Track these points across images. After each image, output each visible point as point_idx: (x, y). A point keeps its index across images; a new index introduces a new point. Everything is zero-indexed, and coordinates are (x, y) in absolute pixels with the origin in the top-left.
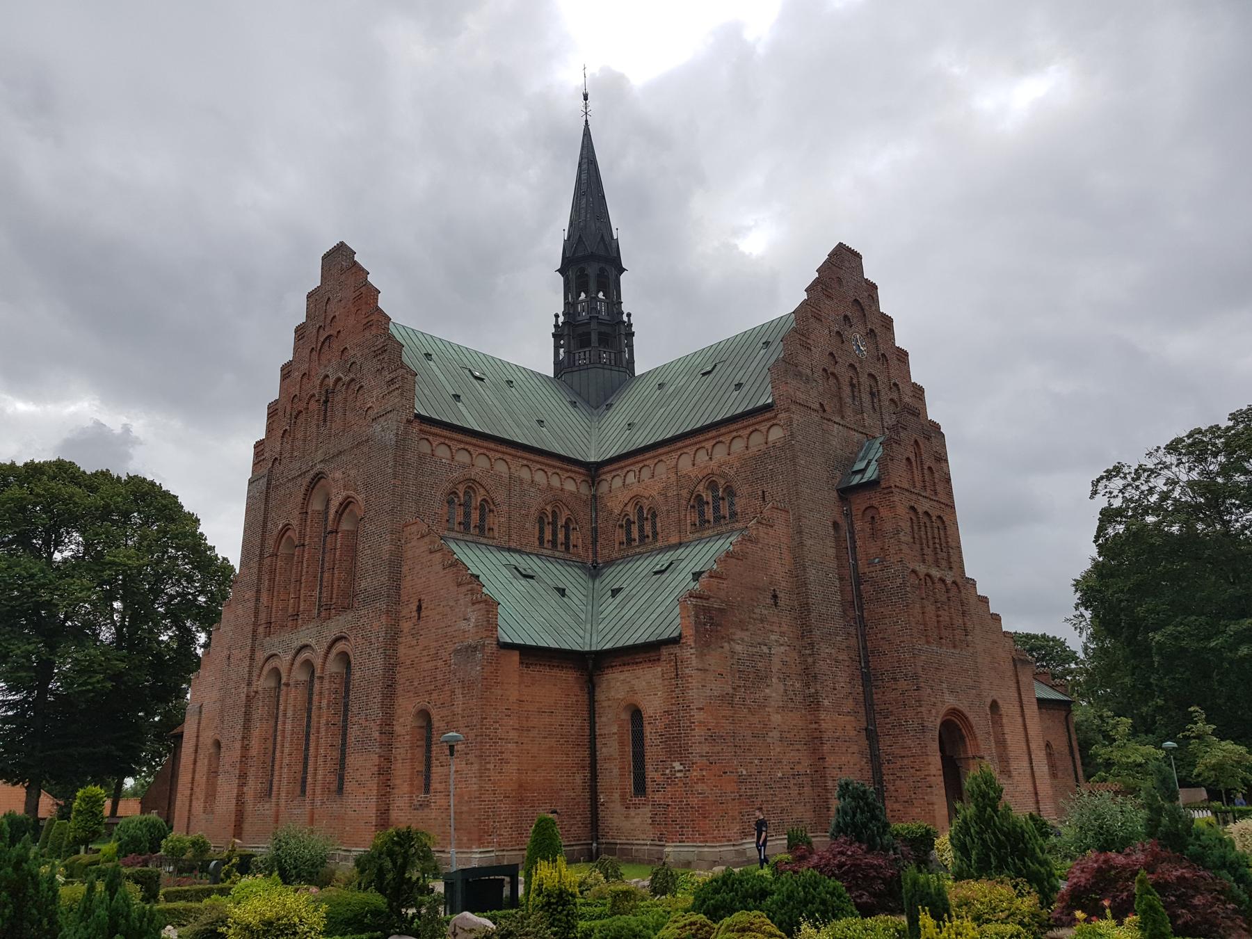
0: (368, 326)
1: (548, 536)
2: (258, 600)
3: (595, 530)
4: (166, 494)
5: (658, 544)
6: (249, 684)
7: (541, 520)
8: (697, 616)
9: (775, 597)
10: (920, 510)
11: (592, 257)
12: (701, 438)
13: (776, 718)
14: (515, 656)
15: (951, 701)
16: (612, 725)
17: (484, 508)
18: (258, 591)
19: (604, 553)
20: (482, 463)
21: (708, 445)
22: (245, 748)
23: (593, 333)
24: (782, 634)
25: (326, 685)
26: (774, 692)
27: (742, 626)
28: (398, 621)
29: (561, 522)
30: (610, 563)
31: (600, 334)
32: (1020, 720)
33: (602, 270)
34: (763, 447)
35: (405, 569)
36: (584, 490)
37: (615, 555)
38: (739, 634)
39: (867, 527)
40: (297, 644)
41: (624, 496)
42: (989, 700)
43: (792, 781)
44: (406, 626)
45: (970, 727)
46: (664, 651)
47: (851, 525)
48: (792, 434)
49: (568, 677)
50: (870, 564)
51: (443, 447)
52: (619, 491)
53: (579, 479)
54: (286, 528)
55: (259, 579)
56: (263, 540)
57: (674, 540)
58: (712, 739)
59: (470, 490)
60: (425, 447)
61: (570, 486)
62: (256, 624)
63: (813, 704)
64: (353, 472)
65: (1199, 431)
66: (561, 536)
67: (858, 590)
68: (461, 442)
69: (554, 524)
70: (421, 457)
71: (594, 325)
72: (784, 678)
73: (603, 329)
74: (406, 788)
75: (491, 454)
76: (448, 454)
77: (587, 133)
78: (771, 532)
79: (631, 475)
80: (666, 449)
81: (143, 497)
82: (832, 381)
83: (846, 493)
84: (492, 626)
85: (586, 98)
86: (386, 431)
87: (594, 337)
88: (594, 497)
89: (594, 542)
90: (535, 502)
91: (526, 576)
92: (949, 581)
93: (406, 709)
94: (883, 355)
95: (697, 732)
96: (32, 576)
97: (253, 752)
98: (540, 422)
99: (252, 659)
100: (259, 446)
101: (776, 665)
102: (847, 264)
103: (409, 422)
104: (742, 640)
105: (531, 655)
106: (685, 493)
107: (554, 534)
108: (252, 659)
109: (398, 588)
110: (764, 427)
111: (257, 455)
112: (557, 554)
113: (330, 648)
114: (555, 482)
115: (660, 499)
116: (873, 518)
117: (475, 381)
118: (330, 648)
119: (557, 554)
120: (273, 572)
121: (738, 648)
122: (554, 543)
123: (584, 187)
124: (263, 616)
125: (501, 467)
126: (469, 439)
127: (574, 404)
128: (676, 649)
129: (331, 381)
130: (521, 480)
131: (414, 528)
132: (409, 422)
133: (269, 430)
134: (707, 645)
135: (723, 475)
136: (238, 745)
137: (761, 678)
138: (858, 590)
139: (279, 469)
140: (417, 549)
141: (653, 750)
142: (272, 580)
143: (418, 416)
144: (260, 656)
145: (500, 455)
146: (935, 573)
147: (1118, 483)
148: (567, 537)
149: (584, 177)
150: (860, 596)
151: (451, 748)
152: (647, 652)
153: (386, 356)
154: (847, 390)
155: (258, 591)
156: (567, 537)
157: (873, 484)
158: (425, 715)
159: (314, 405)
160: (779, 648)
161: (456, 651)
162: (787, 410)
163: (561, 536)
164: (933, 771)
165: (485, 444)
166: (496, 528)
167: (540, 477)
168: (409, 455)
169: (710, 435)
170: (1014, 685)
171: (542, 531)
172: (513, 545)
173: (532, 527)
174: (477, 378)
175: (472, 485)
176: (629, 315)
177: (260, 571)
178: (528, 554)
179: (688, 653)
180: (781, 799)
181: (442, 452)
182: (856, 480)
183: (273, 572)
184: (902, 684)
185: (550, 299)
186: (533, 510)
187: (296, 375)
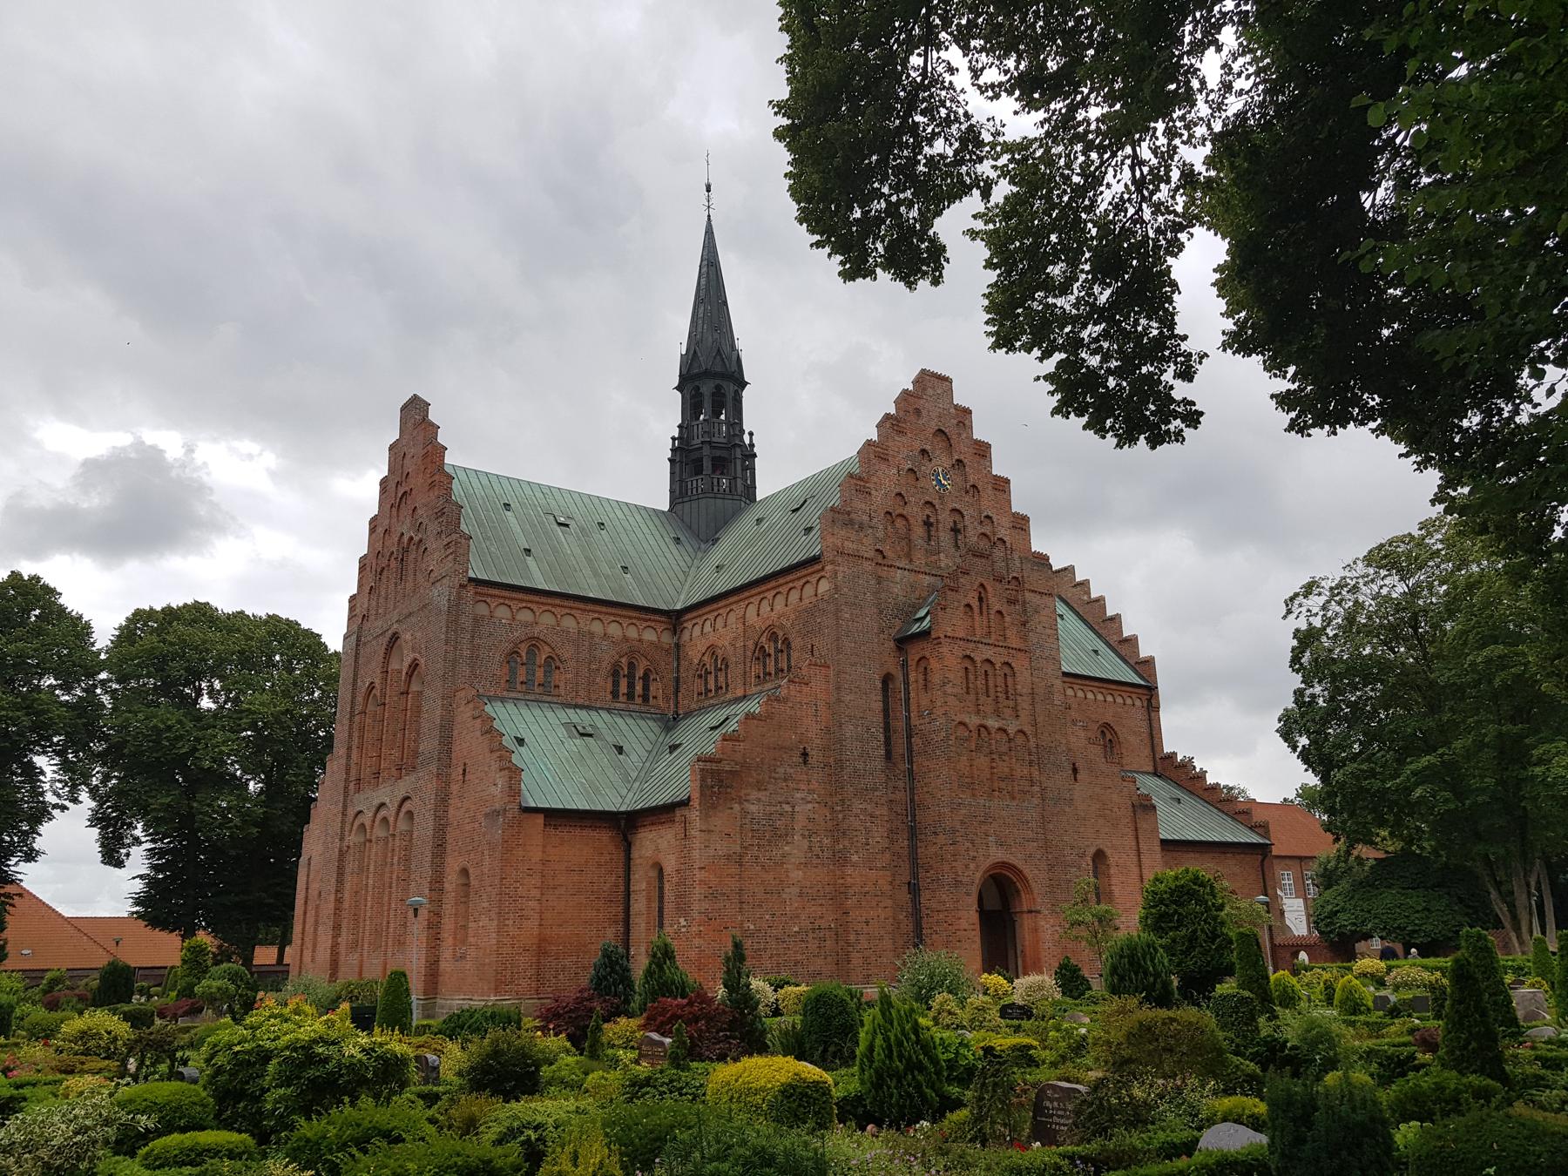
0: (432, 485)
1: (623, 688)
2: (349, 757)
3: (677, 680)
4: (309, 634)
5: (729, 696)
6: (342, 839)
7: (615, 673)
8: (703, 780)
9: (805, 754)
10: (978, 659)
11: (707, 374)
12: (764, 588)
13: (797, 875)
14: (540, 819)
15: (998, 855)
16: (641, 882)
17: (552, 663)
18: (349, 748)
19: (684, 702)
20: (548, 619)
21: (770, 595)
22: (339, 901)
23: (711, 456)
24: (810, 792)
25: (397, 843)
26: (795, 849)
27: (760, 786)
28: (448, 784)
29: (640, 673)
30: (688, 714)
31: (713, 459)
32: (1135, 870)
33: (718, 387)
34: (814, 599)
35: (455, 733)
36: (667, 638)
37: (694, 706)
38: (754, 794)
39: (921, 677)
40: (376, 802)
41: (701, 646)
42: (1092, 850)
43: (811, 935)
44: (455, 788)
46: (678, 812)
47: (906, 676)
48: (836, 587)
49: (604, 837)
50: (921, 716)
51: (503, 608)
52: (698, 638)
53: (660, 628)
54: (372, 687)
55: (350, 736)
56: (354, 697)
57: (740, 693)
58: (712, 896)
60: (482, 609)
61: (649, 636)
62: (346, 780)
63: (840, 859)
64: (418, 635)
65: (1382, 545)
66: (639, 688)
67: (909, 743)
68: (522, 601)
69: (631, 676)
70: (477, 620)
71: (706, 450)
72: (809, 835)
73: (718, 453)
74: (450, 941)
75: (557, 610)
76: (509, 615)
77: (709, 232)
78: (805, 689)
79: (765, 602)
80: (735, 598)
81: (283, 637)
82: (900, 523)
83: (903, 642)
84: (514, 791)
85: (708, 190)
86: (440, 595)
87: (707, 464)
88: (678, 646)
89: (677, 691)
90: (607, 655)
91: (582, 735)
92: (1012, 730)
93: (453, 865)
94: (974, 486)
95: (697, 890)
96: (169, 728)
97: (346, 905)
98: (625, 568)
99: (344, 814)
100: (352, 599)
101: (800, 822)
102: (930, 391)
103: (461, 586)
104: (759, 800)
105: (556, 817)
106: (750, 644)
107: (631, 686)
108: (344, 814)
109: (450, 751)
110: (813, 579)
111: (351, 609)
112: (632, 707)
113: (400, 806)
114: (632, 633)
115: (730, 650)
117: (556, 526)
118: (400, 806)
119: (632, 707)
120: (362, 729)
121: (753, 808)
122: (630, 696)
123: (702, 294)
124: (353, 772)
125: (569, 623)
126: (531, 597)
127: (677, 540)
128: (685, 811)
129: (406, 538)
130: (592, 634)
131: (462, 694)
132: (461, 586)
133: (360, 586)
134: (713, 806)
135: (782, 627)
136: (332, 897)
137: (783, 836)
138: (909, 743)
139: (367, 625)
140: (464, 713)
141: (669, 907)
142: (361, 737)
143: (471, 580)
144: (351, 812)
146: (992, 723)
147: (1315, 602)
148: (646, 688)
149: (703, 281)
150: (910, 750)
151: (416, 910)
152: (664, 813)
153: (443, 519)
154: (919, 531)
155: (349, 748)
156: (646, 688)
157: (925, 634)
158: (465, 872)
159: (393, 564)
160: (805, 805)
161: (487, 815)
162: (832, 562)
163: (639, 688)
164: (964, 924)
165: (549, 601)
166: (562, 685)
167: (614, 630)
168: (463, 619)
169: (770, 586)
170: (1131, 833)
171: (616, 684)
172: (580, 701)
173: (604, 683)
174: (560, 524)
175: (534, 643)
176: (751, 434)
177: (351, 727)
178: (596, 709)
179: (694, 814)
181: (502, 612)
182: (915, 628)
183: (362, 729)
184: (941, 839)
185: (663, 418)
186: (604, 664)
187: (380, 530)
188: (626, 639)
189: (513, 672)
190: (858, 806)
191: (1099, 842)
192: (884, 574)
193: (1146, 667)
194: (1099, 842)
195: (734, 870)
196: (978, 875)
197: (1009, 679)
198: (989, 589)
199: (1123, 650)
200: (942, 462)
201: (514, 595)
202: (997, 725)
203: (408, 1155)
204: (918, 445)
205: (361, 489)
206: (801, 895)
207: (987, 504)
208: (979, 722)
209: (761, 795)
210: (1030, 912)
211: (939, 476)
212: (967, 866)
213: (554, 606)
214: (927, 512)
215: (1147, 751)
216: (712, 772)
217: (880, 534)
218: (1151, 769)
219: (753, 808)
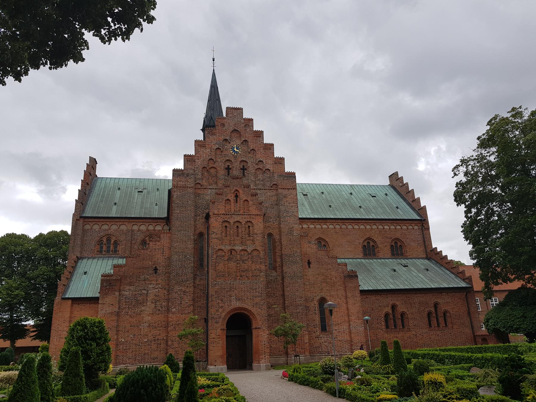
10: (232, 221)
13: (147, 318)
14: (70, 302)
15: (236, 304)
17: (116, 243)
26: (149, 308)
27: (130, 284)
38: (128, 287)
43: (153, 342)
45: (253, 314)
59: (109, 240)
72: (155, 302)
77: (214, 75)
85: (214, 60)
92: (249, 250)
104: (130, 290)
107: (109, 247)
116: (237, 226)
126: (107, 220)
130: (133, 231)
134: (106, 294)
137: (143, 303)
145: (121, 223)
146: (238, 248)
165: (121, 220)
180: (145, 350)
188: (148, 230)
189: (102, 248)
190: (177, 288)
191: (322, 294)
192: (201, 192)
193: (422, 211)
194: (322, 294)
195: (115, 318)
196: (224, 314)
197: (251, 228)
198: (241, 191)
199: (414, 205)
200: (236, 143)
201: (100, 220)
202: (241, 248)
203: (409, 401)
204: (222, 138)
205: (71, 192)
206: (149, 326)
207: (260, 156)
208: (230, 248)
209: (131, 288)
210: (256, 328)
211: (235, 147)
212: (217, 311)
213: (117, 222)
214: (228, 164)
215: (422, 248)
216: (107, 280)
217: (199, 176)
218: (424, 256)
219: (127, 293)
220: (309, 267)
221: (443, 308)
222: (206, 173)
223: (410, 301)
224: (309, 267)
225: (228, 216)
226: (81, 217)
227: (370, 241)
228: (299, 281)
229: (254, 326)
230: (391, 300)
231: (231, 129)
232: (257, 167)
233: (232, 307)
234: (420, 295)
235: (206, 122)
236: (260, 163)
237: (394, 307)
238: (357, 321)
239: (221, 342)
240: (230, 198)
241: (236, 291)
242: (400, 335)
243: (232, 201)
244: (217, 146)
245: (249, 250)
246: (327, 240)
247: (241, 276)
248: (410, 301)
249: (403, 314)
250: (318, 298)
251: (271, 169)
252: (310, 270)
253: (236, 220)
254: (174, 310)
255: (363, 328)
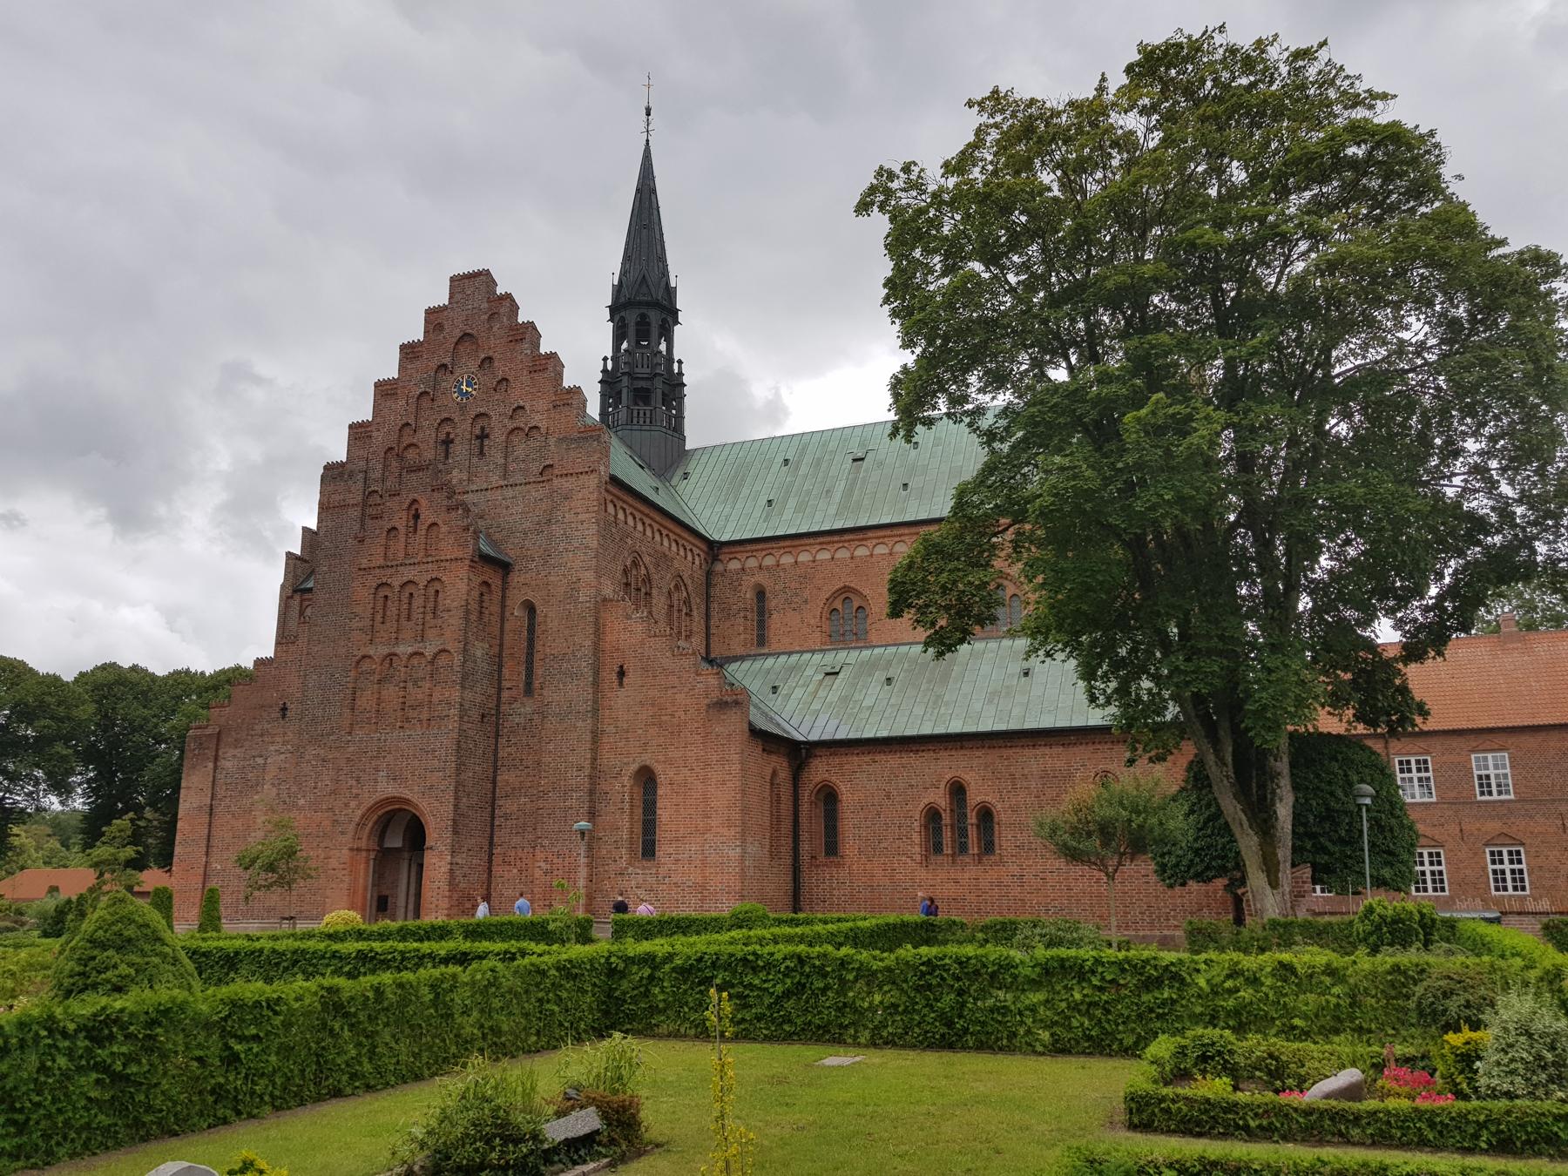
27: (237, 744)
38: (231, 752)
165: (895, 532)
196: (359, 813)
198: (424, 502)
202: (410, 650)
204: (434, 363)
212: (347, 805)
214: (448, 429)
220: (621, 684)
221: (976, 795)
222: (394, 464)
223: (1012, 769)
224: (621, 684)
225: (390, 571)
226: (295, 591)
227: (1006, 583)
228: (580, 724)
229: (427, 844)
230: (951, 766)
231: (458, 333)
232: (511, 425)
233: (379, 796)
234: (1047, 750)
235: (624, 290)
236: (520, 412)
237: (958, 790)
238: (725, 831)
239: (347, 879)
240: (397, 525)
241: (390, 758)
242: (967, 875)
243: (402, 530)
244: (422, 388)
245: (429, 651)
246: (866, 592)
247: (408, 720)
248: (1012, 769)
249: (986, 815)
250: (634, 767)
251: (543, 425)
252: (622, 693)
253: (405, 579)
254: (302, 802)
255: (738, 850)
